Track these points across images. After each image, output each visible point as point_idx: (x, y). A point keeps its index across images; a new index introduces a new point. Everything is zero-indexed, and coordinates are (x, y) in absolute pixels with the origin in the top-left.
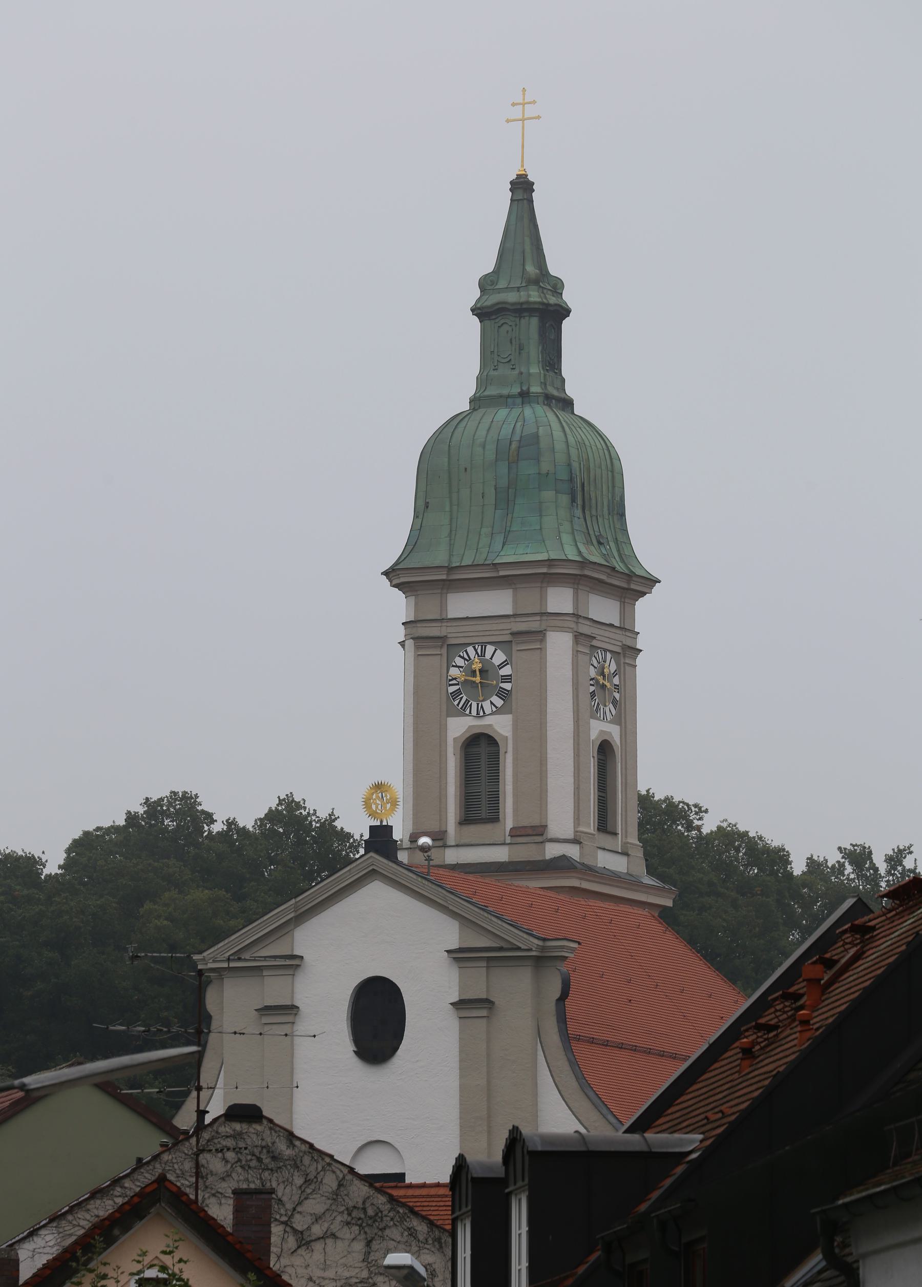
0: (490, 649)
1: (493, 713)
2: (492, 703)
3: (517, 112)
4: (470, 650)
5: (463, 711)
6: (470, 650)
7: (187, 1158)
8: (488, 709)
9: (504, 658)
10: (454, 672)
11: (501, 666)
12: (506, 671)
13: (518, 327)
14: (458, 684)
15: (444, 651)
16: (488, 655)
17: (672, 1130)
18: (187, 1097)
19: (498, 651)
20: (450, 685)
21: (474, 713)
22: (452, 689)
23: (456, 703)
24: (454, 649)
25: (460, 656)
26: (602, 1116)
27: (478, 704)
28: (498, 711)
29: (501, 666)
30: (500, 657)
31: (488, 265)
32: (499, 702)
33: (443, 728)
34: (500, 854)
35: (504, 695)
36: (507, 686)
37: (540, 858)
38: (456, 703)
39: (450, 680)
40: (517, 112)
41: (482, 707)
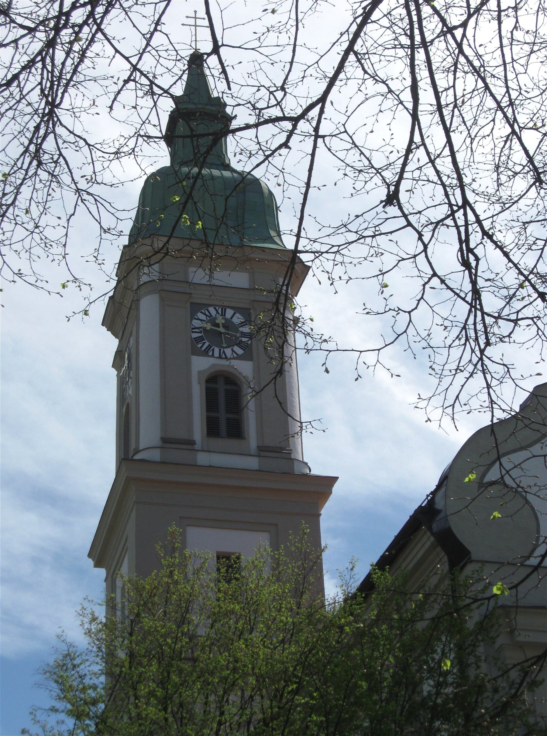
0: (229, 313)
2: (233, 351)
3: (192, 21)
4: (211, 309)
5: (205, 353)
6: (211, 309)
8: (228, 351)
10: (196, 323)
11: (242, 324)
14: (201, 332)
19: (237, 315)
20: (193, 332)
22: (194, 335)
23: (199, 346)
24: (196, 308)
25: (202, 312)
27: (220, 350)
28: (239, 357)
30: (238, 319)
32: (240, 351)
33: (188, 364)
34: (252, 463)
38: (199, 346)
39: (193, 329)
40: (192, 21)
41: (224, 352)
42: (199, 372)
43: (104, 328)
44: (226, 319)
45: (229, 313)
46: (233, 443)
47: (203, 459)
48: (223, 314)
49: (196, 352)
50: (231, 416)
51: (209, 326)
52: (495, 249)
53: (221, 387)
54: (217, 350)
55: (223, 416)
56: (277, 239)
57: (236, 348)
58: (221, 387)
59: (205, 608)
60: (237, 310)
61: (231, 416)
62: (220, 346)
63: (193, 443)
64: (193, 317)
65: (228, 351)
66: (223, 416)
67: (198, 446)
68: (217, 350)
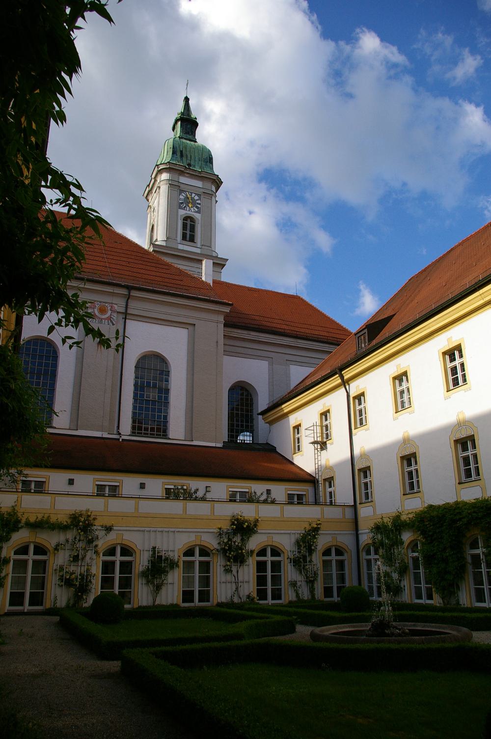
1: (194, 212)
5: (184, 209)
8: (192, 209)
9: (198, 198)
11: (197, 200)
15: (179, 191)
16: (193, 196)
21: (188, 210)
22: (180, 201)
24: (181, 191)
28: (196, 212)
30: (197, 197)
32: (197, 210)
33: (177, 212)
35: (197, 207)
37: (219, 280)
49: (180, 208)
53: (189, 222)
65: (192, 209)
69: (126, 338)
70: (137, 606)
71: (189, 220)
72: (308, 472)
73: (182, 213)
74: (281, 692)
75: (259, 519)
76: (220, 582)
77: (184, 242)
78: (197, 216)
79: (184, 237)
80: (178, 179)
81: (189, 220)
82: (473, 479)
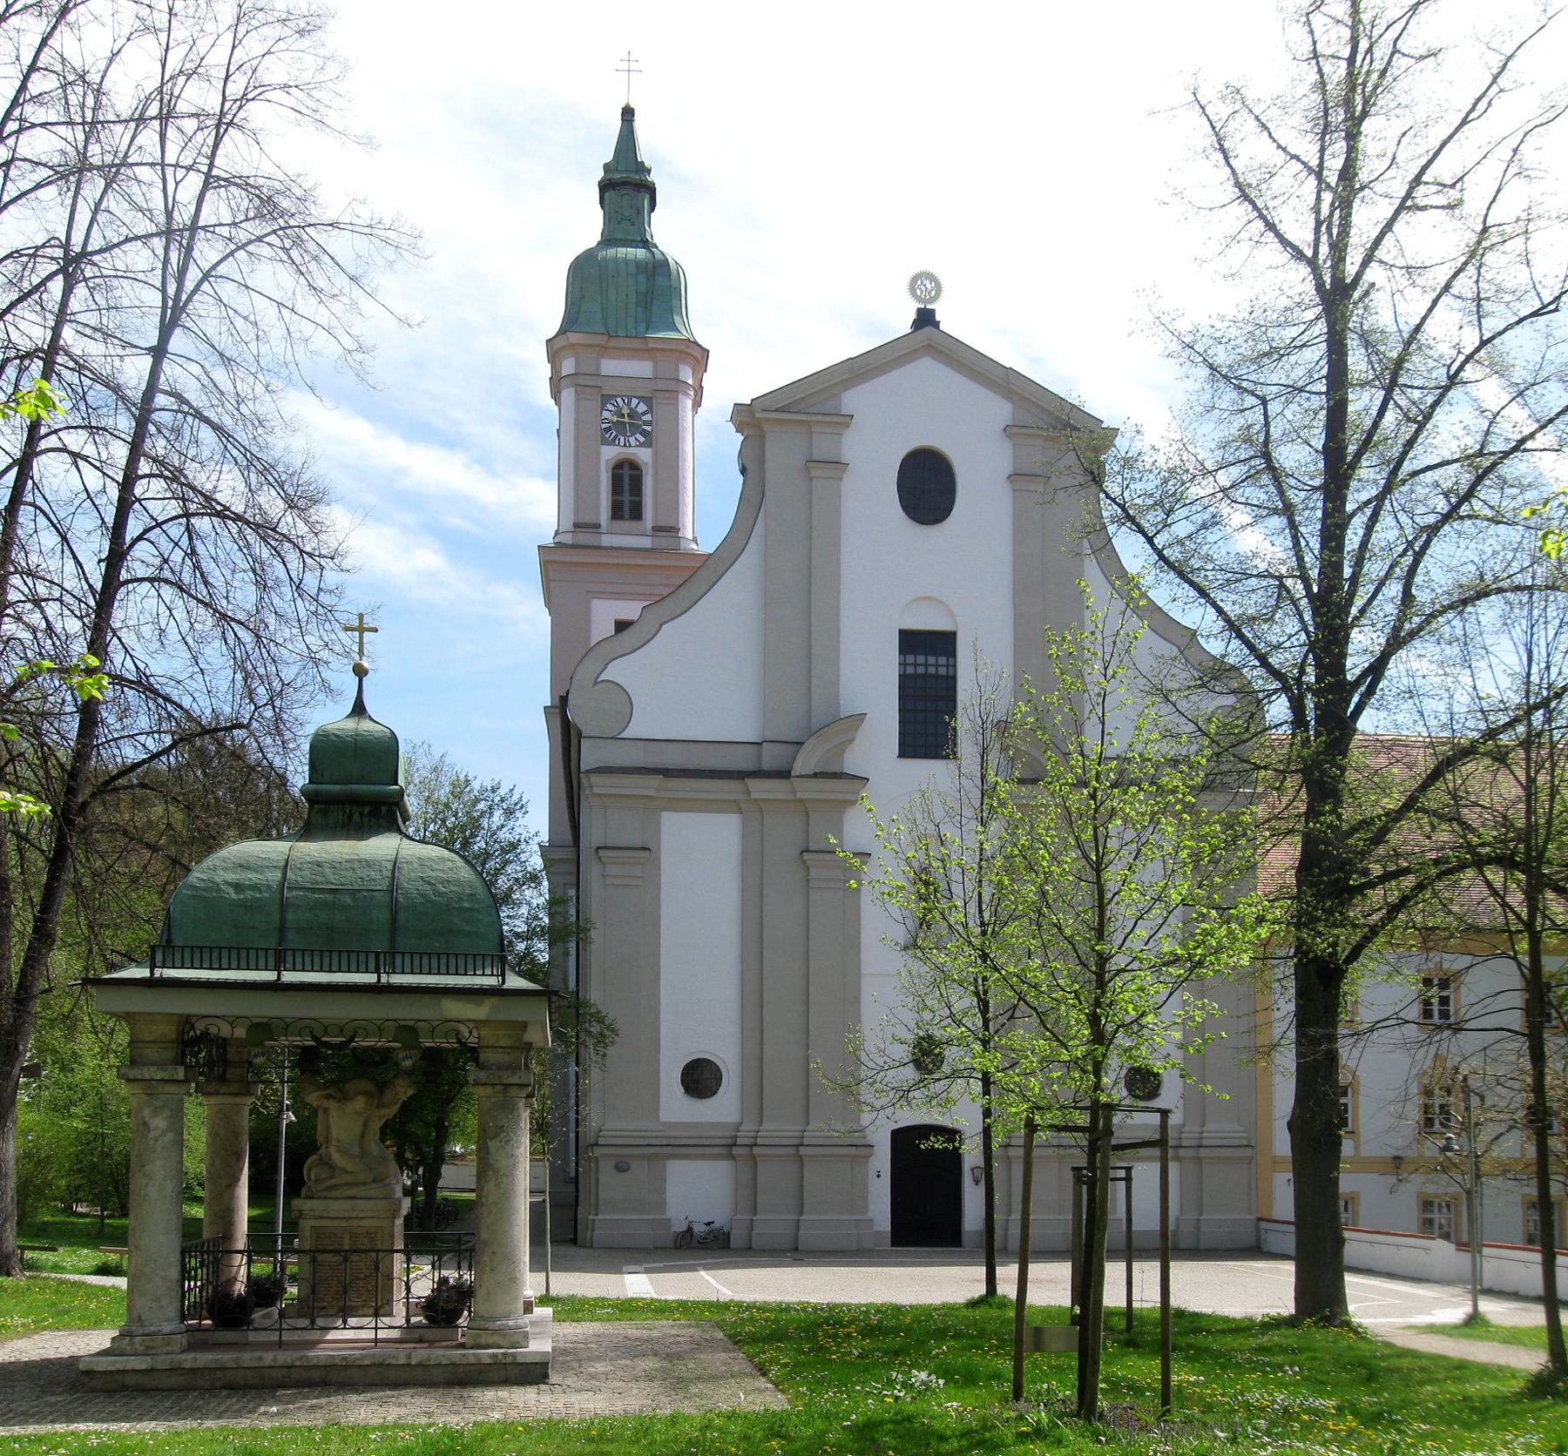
0: (635, 402)
3: (625, 66)
4: (619, 400)
5: (613, 443)
6: (619, 400)
7: (1519, 964)
8: (632, 440)
10: (606, 414)
11: (645, 413)
12: (648, 417)
13: (322, 109)
16: (633, 405)
17: (713, 1278)
18: (857, 730)
22: (604, 426)
24: (606, 399)
26: (1496, 1288)
28: (641, 445)
29: (645, 413)
30: (642, 408)
31: (609, 157)
32: (642, 439)
33: (598, 455)
34: (646, 542)
35: (644, 433)
36: (648, 428)
40: (625, 66)
42: (607, 461)
43: (647, 164)
44: (631, 409)
45: (635, 402)
46: (634, 524)
47: (606, 540)
48: (629, 404)
49: (605, 442)
50: (633, 498)
51: (615, 419)
52: (924, 285)
53: (626, 472)
54: (622, 439)
55: (626, 498)
56: (680, 326)
57: (638, 436)
58: (626, 472)
59: (43, 1131)
60: (641, 399)
61: (633, 498)
62: (625, 436)
63: (598, 526)
64: (603, 408)
65: (632, 440)
66: (626, 498)
67: (603, 529)
68: (622, 439)
69: (159, 285)
70: (980, 1083)
71: (626, 466)
72: (846, 672)
73: (610, 453)
74: (1077, 986)
75: (910, 1073)
76: (123, 729)
77: (619, 525)
78: (644, 455)
79: (617, 513)
80: (598, 367)
81: (626, 466)
82: (1434, 1129)
